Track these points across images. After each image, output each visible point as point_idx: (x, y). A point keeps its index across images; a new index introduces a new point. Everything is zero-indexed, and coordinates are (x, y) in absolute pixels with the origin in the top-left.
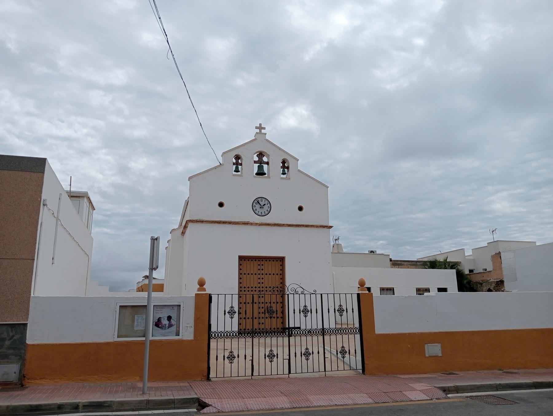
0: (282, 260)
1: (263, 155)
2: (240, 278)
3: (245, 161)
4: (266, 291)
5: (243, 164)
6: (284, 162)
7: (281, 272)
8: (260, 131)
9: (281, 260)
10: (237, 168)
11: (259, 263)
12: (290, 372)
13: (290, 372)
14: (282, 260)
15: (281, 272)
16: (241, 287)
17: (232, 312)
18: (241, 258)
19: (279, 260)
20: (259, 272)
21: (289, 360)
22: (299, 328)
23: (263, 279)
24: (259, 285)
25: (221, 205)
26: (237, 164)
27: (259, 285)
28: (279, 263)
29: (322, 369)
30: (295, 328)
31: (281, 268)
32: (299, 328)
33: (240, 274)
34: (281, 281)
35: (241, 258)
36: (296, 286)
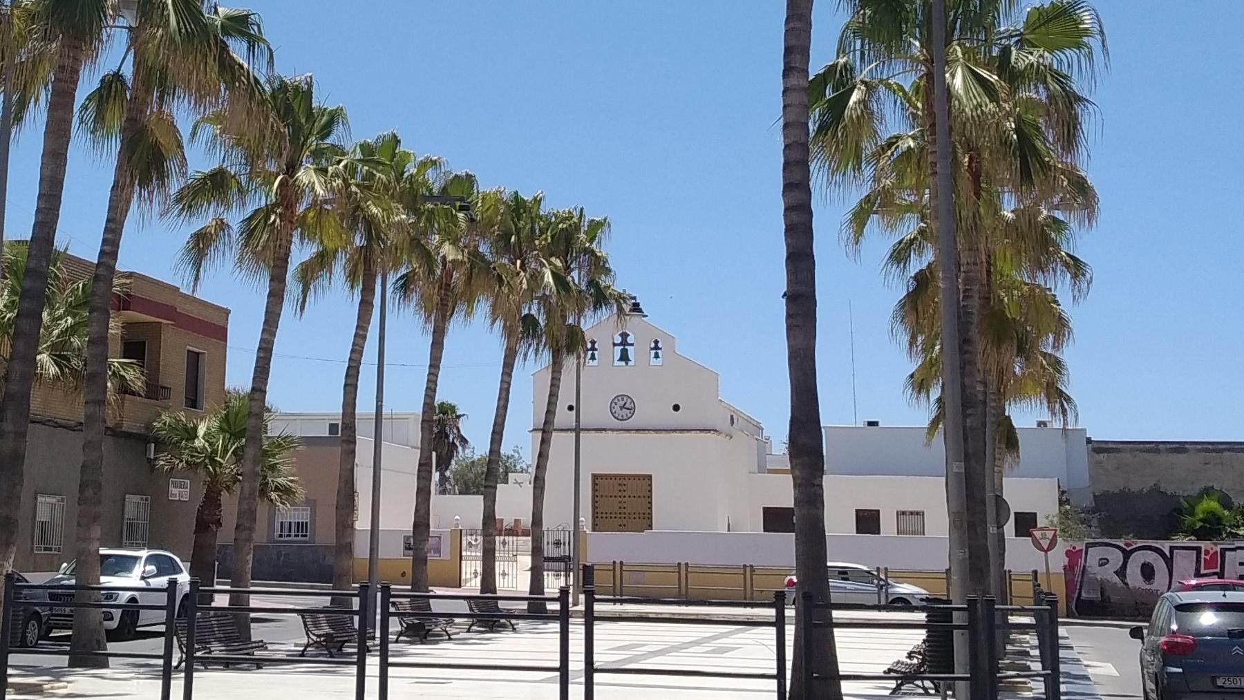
0: (650, 477)
14: (650, 477)
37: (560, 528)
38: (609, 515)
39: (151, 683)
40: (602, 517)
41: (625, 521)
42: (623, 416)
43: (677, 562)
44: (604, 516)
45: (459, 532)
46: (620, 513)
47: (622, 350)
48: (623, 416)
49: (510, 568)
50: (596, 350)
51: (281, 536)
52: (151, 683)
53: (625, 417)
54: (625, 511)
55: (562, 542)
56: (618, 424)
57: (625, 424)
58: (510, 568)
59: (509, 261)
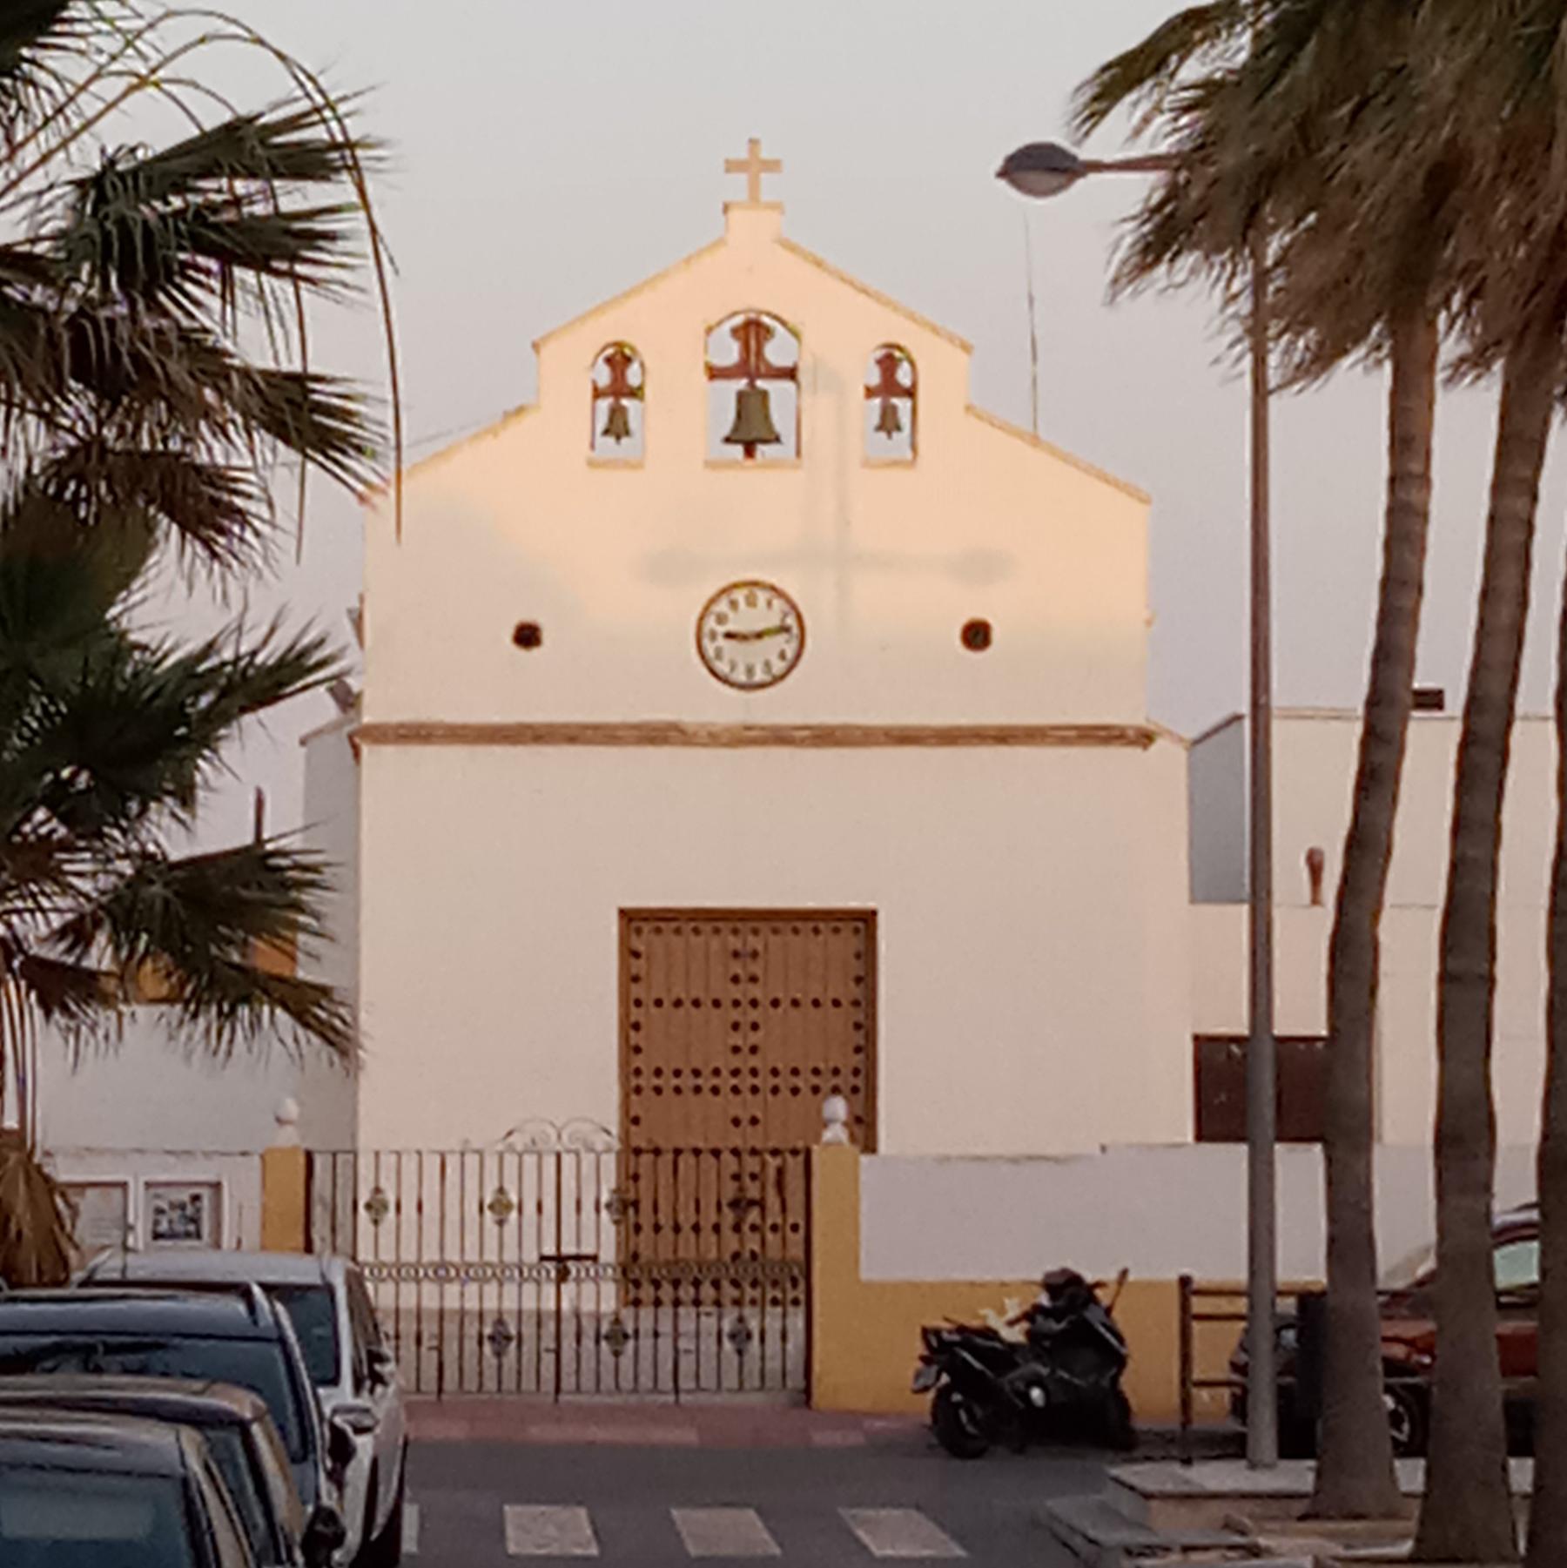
0: (866, 920)
1: (762, 332)
2: (629, 1027)
3: (651, 372)
4: (775, 1090)
5: (648, 391)
6: (888, 363)
7: (857, 992)
8: (754, 187)
9: (860, 925)
10: (617, 414)
11: (735, 943)
12: (558, 1390)
13: (558, 1390)
14: (866, 920)
15: (857, 992)
16: (638, 1072)
17: (377, 1207)
18: (628, 917)
19: (847, 927)
20: (736, 992)
21: (558, 1353)
22: (594, 1258)
23: (755, 1027)
24: (736, 1061)
25: (527, 636)
26: (620, 389)
27: (736, 1061)
28: (847, 942)
29: (666, 1381)
30: (578, 1258)
31: (857, 968)
32: (594, 1258)
33: (629, 1002)
34: (859, 1038)
35: (628, 917)
36: (586, 1127)
37: (518, 1141)
38: (687, 1081)
39: (382, 205)
40: (698, 1089)
41: (754, 1106)
42: (750, 671)
43: (1173, 1276)
44: (706, 1082)
45: (302, 1160)
46: (735, 1073)
47: (741, 396)
48: (750, 671)
49: (588, 1364)
50: (636, 393)
51: (713, 636)
52: (382, 205)
53: (759, 676)
54: (754, 1061)
55: (391, 1198)
56: (730, 708)
57: (767, 709)
58: (588, 1364)
59: (85, 298)
